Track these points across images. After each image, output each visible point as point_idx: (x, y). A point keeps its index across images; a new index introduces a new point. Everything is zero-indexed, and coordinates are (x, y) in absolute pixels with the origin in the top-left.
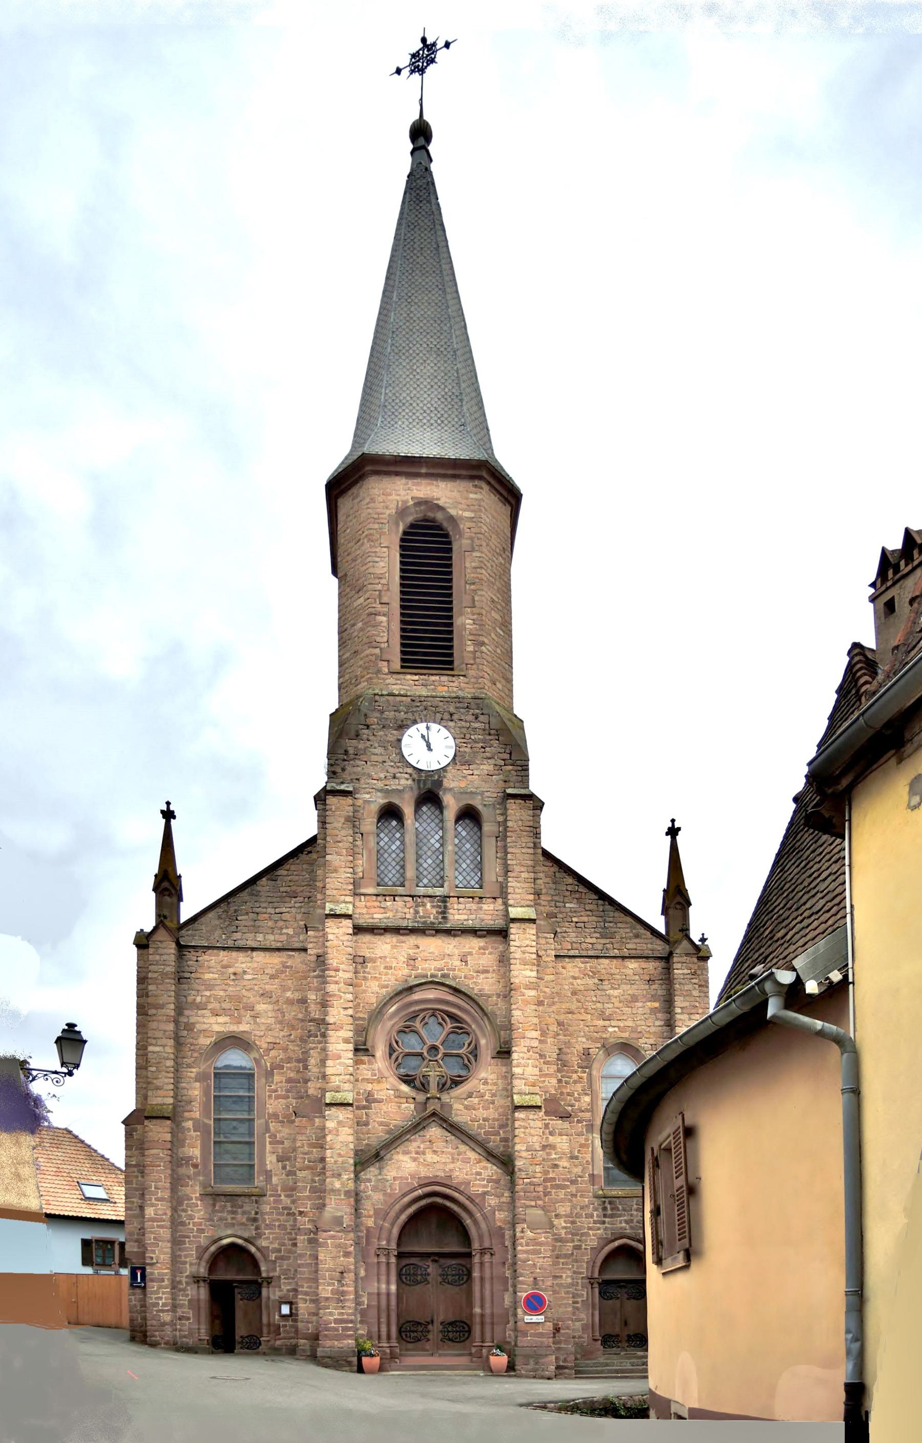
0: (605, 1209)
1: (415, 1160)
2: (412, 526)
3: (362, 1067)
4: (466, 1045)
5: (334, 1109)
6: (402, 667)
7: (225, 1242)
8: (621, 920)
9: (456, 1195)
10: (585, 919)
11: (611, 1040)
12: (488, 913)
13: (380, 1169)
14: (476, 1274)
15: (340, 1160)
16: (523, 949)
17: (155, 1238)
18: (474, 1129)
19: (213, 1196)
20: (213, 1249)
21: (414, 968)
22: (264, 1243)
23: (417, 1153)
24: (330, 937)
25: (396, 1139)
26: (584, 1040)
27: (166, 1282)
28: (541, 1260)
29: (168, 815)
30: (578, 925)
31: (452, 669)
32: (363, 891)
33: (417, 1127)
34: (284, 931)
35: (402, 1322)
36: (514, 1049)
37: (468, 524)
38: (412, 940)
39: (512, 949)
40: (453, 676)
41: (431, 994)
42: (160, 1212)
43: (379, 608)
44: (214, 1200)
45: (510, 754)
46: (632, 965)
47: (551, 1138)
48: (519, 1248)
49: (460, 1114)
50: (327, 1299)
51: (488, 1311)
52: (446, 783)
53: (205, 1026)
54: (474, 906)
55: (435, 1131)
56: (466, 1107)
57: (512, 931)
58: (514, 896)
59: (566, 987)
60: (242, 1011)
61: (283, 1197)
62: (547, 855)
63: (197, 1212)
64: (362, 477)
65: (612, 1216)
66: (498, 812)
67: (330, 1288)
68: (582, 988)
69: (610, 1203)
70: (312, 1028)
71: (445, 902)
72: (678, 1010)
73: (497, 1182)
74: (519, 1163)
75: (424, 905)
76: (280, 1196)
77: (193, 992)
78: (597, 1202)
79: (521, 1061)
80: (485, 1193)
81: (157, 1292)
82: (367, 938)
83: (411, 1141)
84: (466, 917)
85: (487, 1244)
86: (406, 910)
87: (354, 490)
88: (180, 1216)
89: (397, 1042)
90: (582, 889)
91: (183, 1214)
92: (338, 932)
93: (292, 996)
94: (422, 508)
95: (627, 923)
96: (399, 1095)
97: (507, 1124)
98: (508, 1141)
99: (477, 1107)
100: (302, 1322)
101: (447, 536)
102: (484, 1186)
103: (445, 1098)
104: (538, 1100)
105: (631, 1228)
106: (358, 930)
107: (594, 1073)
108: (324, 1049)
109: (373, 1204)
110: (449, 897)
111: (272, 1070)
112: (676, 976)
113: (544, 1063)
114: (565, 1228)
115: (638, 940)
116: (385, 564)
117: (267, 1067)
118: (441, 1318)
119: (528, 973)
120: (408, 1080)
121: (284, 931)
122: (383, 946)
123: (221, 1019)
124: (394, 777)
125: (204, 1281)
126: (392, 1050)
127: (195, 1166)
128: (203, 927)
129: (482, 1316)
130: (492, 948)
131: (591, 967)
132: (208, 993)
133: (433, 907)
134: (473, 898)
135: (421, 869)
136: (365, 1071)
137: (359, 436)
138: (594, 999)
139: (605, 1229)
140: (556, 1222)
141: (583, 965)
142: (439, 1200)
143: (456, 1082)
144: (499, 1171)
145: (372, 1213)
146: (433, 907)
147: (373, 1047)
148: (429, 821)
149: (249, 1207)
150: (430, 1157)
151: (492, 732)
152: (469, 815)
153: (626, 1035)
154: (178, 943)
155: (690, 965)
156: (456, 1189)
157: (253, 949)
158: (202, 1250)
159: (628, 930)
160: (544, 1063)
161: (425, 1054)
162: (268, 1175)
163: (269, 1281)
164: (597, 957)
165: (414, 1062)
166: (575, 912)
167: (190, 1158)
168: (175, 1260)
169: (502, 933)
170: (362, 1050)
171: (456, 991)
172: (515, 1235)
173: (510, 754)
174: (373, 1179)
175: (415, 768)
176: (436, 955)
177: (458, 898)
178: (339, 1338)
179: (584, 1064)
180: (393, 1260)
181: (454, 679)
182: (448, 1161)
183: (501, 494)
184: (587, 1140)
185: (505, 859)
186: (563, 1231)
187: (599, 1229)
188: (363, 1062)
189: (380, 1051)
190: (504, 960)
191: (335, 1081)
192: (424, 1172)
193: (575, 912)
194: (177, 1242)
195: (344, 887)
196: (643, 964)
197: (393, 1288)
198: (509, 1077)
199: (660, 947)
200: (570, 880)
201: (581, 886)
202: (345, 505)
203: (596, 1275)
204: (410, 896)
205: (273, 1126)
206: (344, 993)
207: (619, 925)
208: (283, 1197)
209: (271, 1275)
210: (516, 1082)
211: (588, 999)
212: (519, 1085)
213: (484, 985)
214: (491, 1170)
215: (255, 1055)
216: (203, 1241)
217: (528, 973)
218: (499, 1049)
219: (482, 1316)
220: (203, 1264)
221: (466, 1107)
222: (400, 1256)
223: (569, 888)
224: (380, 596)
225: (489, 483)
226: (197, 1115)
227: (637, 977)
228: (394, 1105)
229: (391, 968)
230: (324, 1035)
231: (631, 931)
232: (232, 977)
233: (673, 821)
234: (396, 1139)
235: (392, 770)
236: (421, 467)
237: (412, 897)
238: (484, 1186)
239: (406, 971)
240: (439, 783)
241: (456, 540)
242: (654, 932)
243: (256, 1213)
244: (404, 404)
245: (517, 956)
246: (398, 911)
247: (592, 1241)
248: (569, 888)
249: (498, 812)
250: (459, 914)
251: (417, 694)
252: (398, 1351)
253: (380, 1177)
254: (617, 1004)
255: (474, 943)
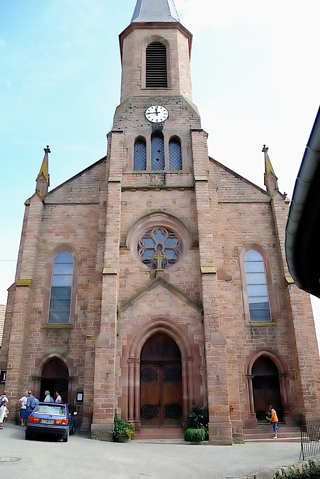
0: (252, 333)
1: (149, 305)
2: (151, 44)
3: (123, 255)
4: (176, 244)
5: (107, 276)
6: (147, 86)
7: (51, 356)
8: (246, 186)
9: (172, 326)
10: (230, 186)
11: (248, 242)
12: (185, 180)
13: (132, 310)
14: (184, 374)
15: (109, 305)
16: (202, 194)
17: (13, 353)
18: (181, 288)
19: (47, 330)
20: (44, 360)
21: (150, 206)
22: (71, 356)
23: (151, 302)
24: (110, 191)
25: (140, 293)
26: (234, 242)
27: (16, 380)
28: (220, 364)
29: (47, 151)
30: (227, 189)
31: (166, 86)
32: (126, 172)
33: (150, 287)
34: (92, 196)
35: (142, 406)
36: (200, 243)
37: (172, 42)
38: (149, 193)
39: (197, 194)
40: (167, 90)
41: (157, 218)
42: (17, 338)
43: (137, 69)
44: (48, 331)
45: (192, 116)
46: (254, 206)
47: (221, 291)
48: (207, 357)
49: (173, 280)
50: (99, 390)
51: (191, 398)
52: (164, 127)
53: (52, 241)
54: (178, 177)
55: (160, 289)
56: (177, 275)
57: (196, 186)
58: (197, 171)
59: (224, 217)
60: (69, 233)
61: (82, 330)
62: (210, 158)
63: (39, 338)
64: (132, 31)
65: (256, 338)
66: (188, 138)
67: (101, 384)
68: (231, 217)
69: (254, 330)
70: (100, 237)
71: (165, 176)
72: (278, 226)
73: (194, 317)
74: (205, 306)
75: (155, 177)
76: (81, 329)
77: (48, 225)
78: (248, 330)
79: (204, 249)
80: (188, 324)
81: (10, 387)
82: (127, 193)
83: (147, 295)
84: (175, 182)
85: (189, 354)
86: (147, 180)
87: (129, 35)
88: (29, 341)
89: (142, 244)
90: (228, 173)
91: (31, 340)
92: (114, 190)
93: (93, 225)
94: (154, 38)
95: (250, 187)
96: (141, 270)
97: (198, 284)
98: (199, 295)
99: (182, 275)
100: (86, 406)
101: (164, 46)
102: (187, 320)
103: (165, 271)
104: (213, 270)
105: (267, 344)
106: (124, 189)
107: (241, 259)
108: (104, 247)
109: (127, 332)
110: (166, 174)
111: (81, 261)
112: (275, 210)
113: (216, 251)
114: (232, 344)
115: (255, 195)
116: (141, 57)
117: (79, 260)
118: (165, 403)
119: (205, 206)
120: (146, 262)
121: (92, 196)
122: (135, 196)
123: (59, 237)
124: (142, 126)
125: (39, 379)
126: (139, 247)
127: (40, 313)
128: (56, 195)
129: (188, 401)
130: (187, 196)
131: (235, 208)
132: (55, 225)
133: (159, 178)
134: (177, 174)
135: (154, 163)
136: (125, 258)
137: (133, 19)
138: (238, 223)
139: (253, 345)
140: (227, 340)
141: (231, 207)
142: (162, 329)
143: (172, 262)
144: (196, 311)
145: (126, 337)
146: (159, 178)
147: (129, 245)
148: (157, 143)
149: (65, 335)
150: (158, 304)
151: (184, 108)
152: (175, 140)
153: (254, 240)
154: (43, 202)
155: (281, 205)
156: (172, 322)
157: (77, 204)
158: (38, 361)
159: (250, 191)
160: (216, 251)
161: (156, 249)
162: (76, 317)
163: (72, 379)
164: (238, 203)
165: (151, 253)
166: (225, 183)
167: (38, 308)
168: (23, 365)
169: (192, 188)
170: (123, 246)
171: (170, 216)
172: (205, 349)
173: (192, 116)
174: (127, 317)
175: (151, 122)
176: (161, 200)
177: (171, 174)
178: (104, 417)
179: (236, 255)
180: (138, 366)
181: (167, 91)
182: (167, 306)
183: (184, 35)
184: (239, 295)
185: (192, 156)
186: (231, 346)
187: (250, 346)
188: (124, 253)
189: (133, 247)
190: (194, 201)
191: (108, 262)
192: (156, 313)
193: (225, 183)
194: (26, 356)
195: (118, 170)
196: (259, 206)
197: (138, 383)
198: (198, 259)
199: (266, 198)
200: (222, 170)
201: (227, 172)
202: (125, 41)
203: (250, 373)
204: (148, 174)
205: (80, 291)
206: (115, 218)
207: (246, 188)
208: (82, 330)
209: (74, 375)
210: (202, 261)
211: (235, 223)
212: (203, 262)
213: (184, 213)
214: (191, 310)
215: (73, 254)
216: (40, 355)
217: (205, 206)
218: (193, 244)
219: (188, 401)
220: (39, 369)
221: (177, 276)
222: (142, 363)
223: (222, 173)
224: (138, 65)
225: (180, 30)
226: (43, 285)
227: (257, 212)
228: (140, 275)
229: (139, 207)
230: (104, 240)
231: (252, 191)
232: (67, 217)
233: (264, 145)
234: (140, 293)
235: (141, 123)
236: (154, 26)
237: (150, 174)
238: (187, 320)
239: (146, 208)
240: (162, 127)
241: (167, 47)
242: (262, 191)
243: (68, 339)
244: (148, 11)
245: (199, 197)
246: (143, 181)
247: (246, 352)
248: (222, 173)
249: (188, 138)
250: (171, 181)
251: (152, 96)
252: (140, 425)
253: (131, 316)
254: (249, 225)
255: (178, 194)
